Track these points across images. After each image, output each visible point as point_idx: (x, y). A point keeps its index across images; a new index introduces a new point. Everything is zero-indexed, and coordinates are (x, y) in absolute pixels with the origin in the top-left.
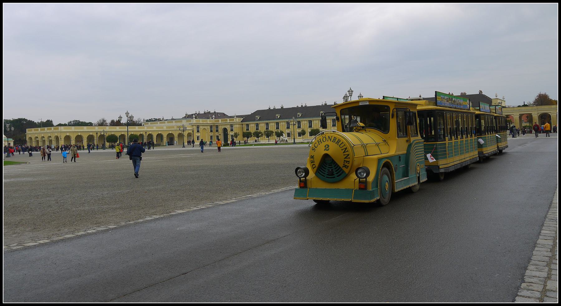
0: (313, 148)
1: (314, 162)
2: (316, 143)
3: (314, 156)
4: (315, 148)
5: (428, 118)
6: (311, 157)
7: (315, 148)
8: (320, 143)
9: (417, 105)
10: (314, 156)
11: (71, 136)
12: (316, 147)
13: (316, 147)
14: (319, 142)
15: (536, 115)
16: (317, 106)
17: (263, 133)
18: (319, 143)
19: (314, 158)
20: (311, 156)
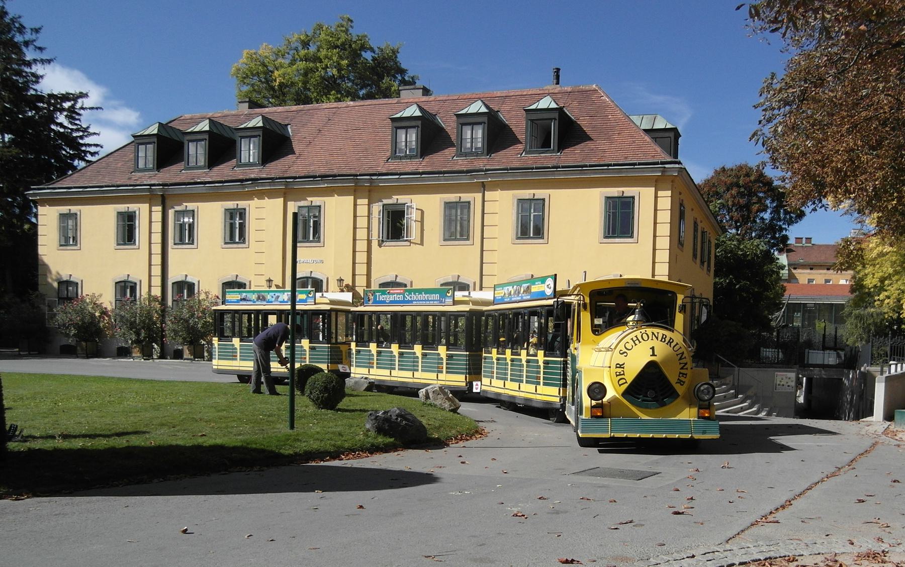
0: (626, 356)
1: (624, 374)
4: (625, 350)
5: (321, 316)
7: (625, 350)
8: (637, 342)
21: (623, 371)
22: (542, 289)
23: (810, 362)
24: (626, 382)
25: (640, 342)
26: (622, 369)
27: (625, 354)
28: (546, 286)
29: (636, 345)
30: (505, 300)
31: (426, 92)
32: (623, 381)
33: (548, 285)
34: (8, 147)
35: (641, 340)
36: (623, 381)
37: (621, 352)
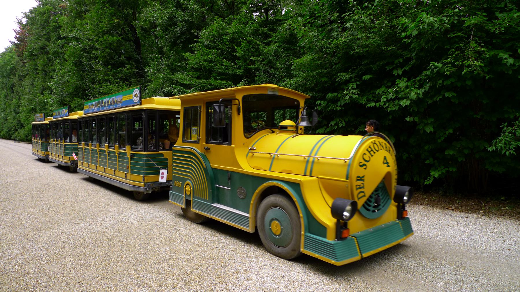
0: (365, 169)
1: (363, 187)
2: (365, 154)
3: (363, 177)
4: (364, 162)
5: (150, 121)
6: (359, 179)
7: (364, 162)
8: (372, 153)
9: (186, 199)
10: (363, 177)
11: (398, 243)
12: (367, 161)
13: (367, 161)
14: (369, 152)
15: (361, 244)
16: (347, 135)
17: (116, 7)
18: (371, 148)
19: (363, 180)
20: (358, 177)
21: (363, 184)
22: (131, 98)
23: (408, 208)
24: (364, 196)
25: (375, 153)
26: (362, 182)
27: (365, 167)
28: (134, 96)
29: (372, 156)
30: (90, 111)
31: (245, 3)
32: (362, 194)
33: (135, 95)
34: (501, 121)
35: (375, 151)
36: (362, 194)
37: (361, 164)
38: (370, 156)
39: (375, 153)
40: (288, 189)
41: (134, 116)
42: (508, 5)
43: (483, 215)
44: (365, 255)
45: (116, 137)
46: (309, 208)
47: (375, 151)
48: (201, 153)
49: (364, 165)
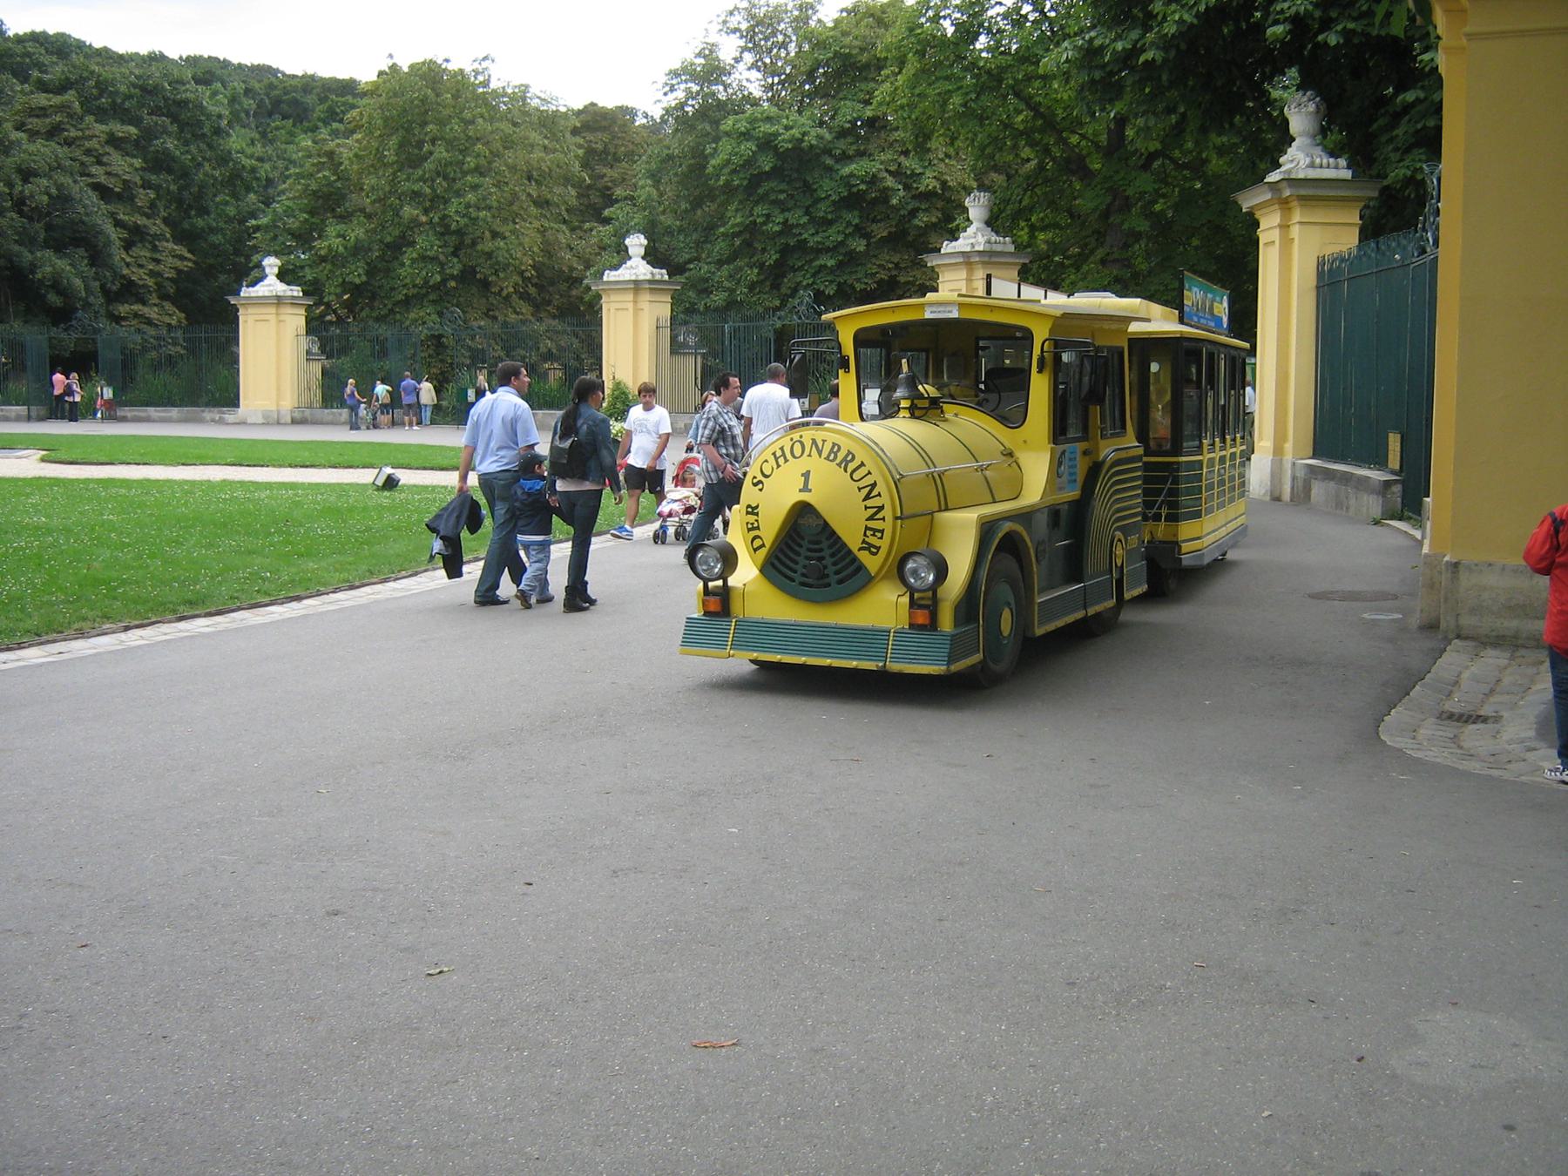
0: (761, 490)
1: (758, 528)
2: (766, 461)
3: (757, 507)
4: (760, 477)
7: (760, 477)
8: (781, 461)
10: (757, 507)
14: (776, 459)
19: (757, 514)
20: (749, 506)
26: (756, 517)
29: (778, 466)
38: (775, 467)
39: (786, 461)
40: (1264, 442)
41: (1247, 345)
42: (995, 84)
43: (1503, 636)
44: (895, 667)
45: (1090, 380)
46: (1013, 513)
47: (788, 456)
48: (1212, 388)
49: (760, 482)
